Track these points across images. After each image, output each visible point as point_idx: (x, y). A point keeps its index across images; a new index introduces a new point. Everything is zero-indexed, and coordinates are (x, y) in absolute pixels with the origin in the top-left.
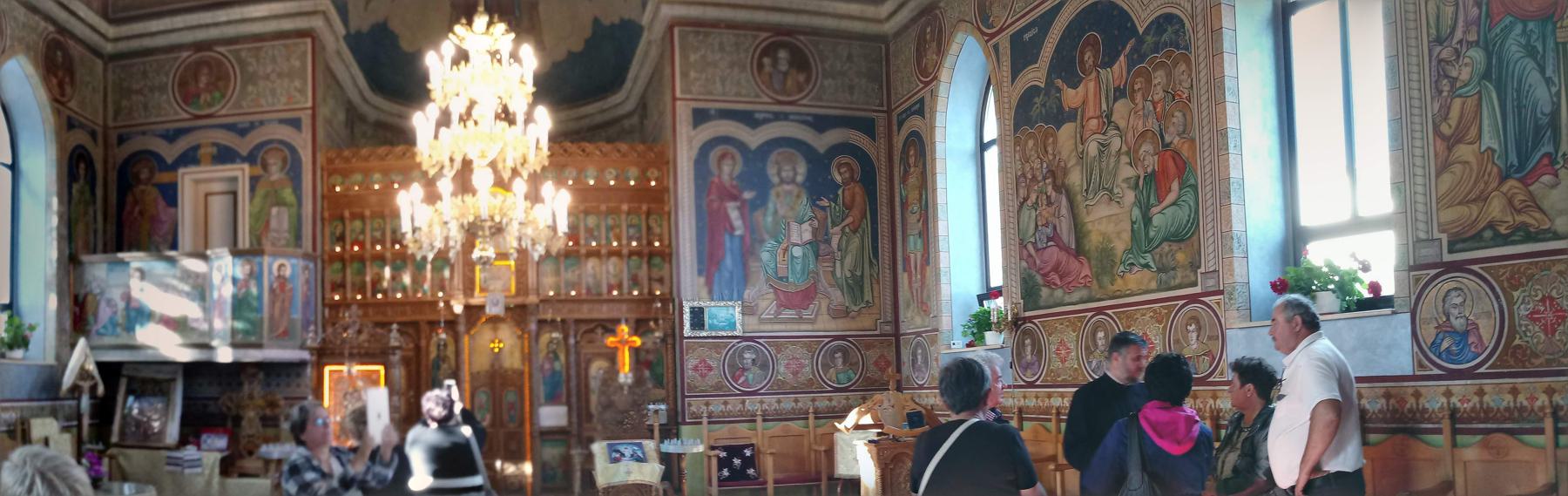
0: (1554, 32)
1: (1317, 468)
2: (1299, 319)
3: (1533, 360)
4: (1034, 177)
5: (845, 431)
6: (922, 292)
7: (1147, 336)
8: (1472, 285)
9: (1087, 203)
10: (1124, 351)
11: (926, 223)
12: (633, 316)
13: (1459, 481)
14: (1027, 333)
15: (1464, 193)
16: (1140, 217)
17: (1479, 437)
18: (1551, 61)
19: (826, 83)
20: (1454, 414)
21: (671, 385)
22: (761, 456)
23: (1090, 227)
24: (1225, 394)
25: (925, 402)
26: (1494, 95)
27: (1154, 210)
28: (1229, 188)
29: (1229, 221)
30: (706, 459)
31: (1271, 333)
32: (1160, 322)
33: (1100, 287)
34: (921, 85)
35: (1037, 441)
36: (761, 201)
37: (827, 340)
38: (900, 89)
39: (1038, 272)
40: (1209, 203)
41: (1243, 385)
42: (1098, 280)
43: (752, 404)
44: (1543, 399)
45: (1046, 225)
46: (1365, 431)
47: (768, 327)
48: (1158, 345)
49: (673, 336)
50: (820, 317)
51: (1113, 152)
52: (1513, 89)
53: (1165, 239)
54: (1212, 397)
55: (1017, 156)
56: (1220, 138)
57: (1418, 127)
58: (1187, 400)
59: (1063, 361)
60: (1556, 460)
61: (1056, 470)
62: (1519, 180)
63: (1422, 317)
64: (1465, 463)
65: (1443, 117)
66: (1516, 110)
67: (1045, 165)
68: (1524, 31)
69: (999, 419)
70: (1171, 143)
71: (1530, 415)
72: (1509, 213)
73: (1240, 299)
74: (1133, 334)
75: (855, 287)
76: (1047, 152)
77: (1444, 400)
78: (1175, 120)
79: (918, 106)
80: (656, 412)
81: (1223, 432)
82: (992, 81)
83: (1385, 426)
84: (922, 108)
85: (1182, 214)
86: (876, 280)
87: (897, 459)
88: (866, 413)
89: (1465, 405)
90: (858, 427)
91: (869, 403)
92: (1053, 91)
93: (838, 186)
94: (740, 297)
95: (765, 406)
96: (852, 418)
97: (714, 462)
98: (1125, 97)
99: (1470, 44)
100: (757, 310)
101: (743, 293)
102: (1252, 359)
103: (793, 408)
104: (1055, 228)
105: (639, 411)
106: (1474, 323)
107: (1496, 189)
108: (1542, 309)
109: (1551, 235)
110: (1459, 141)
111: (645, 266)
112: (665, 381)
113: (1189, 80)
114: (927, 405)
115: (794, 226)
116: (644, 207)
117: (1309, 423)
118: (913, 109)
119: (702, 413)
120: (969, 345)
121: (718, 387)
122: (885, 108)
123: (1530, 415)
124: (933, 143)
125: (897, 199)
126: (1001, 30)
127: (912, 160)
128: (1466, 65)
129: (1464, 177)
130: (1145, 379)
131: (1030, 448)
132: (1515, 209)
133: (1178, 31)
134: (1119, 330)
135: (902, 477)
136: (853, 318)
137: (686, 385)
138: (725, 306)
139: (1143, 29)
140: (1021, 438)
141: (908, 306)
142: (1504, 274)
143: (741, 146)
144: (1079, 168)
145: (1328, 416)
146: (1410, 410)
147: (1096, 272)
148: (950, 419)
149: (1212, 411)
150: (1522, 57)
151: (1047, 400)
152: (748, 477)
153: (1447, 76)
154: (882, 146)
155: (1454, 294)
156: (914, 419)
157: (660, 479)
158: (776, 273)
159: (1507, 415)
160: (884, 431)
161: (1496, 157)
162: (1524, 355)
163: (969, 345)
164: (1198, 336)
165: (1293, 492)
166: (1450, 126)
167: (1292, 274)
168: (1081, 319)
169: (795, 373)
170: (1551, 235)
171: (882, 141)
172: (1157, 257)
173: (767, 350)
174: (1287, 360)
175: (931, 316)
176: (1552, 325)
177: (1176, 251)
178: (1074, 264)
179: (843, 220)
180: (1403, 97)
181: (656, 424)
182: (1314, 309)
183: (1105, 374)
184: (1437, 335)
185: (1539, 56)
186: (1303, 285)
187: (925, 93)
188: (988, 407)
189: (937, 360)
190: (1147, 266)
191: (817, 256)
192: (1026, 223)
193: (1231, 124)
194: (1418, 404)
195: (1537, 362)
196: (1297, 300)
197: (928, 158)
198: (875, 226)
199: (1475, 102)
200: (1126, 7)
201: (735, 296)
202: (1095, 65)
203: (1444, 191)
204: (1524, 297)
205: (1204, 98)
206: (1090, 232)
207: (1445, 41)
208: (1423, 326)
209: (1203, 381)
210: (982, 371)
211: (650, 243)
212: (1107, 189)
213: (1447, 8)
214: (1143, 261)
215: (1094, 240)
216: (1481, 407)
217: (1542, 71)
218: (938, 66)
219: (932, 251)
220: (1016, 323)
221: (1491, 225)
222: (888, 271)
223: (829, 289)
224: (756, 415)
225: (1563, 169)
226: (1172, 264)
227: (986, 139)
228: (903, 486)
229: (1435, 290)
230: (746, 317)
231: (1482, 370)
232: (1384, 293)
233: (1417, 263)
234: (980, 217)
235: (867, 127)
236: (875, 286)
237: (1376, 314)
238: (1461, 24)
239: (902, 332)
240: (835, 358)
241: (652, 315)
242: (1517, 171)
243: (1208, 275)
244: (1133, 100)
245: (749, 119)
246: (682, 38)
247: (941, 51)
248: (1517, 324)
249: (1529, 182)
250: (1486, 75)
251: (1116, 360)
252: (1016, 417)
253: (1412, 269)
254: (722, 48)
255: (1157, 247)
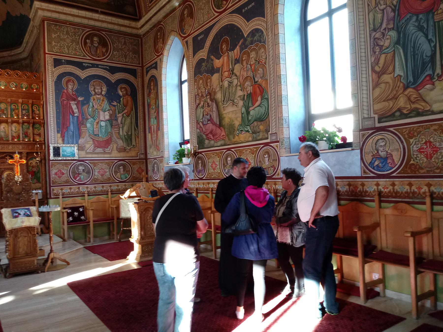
0: (433, 17)
1: (318, 214)
2: (311, 152)
3: (420, 171)
4: (202, 95)
5: (124, 199)
6: (156, 142)
7: (248, 159)
8: (389, 137)
9: (224, 106)
10: (238, 165)
11: (158, 113)
12: (25, 151)
13: (383, 223)
14: (199, 158)
15: (386, 96)
16: (245, 111)
17: (392, 204)
18: (431, 31)
19: (115, 53)
20: (380, 194)
21: (44, 181)
22: (87, 211)
23: (225, 115)
24: (280, 183)
25: (158, 186)
26: (401, 51)
27: (251, 109)
28: (281, 99)
29: (282, 113)
30: (61, 214)
31: (299, 158)
32: (253, 154)
33: (229, 140)
34: (156, 57)
35: (203, 201)
36: (87, 101)
37: (116, 161)
38: (147, 58)
39: (204, 133)
40: (273, 105)
41: (287, 179)
42: (228, 137)
43: (83, 189)
44: (425, 189)
45: (207, 115)
46: (339, 200)
47: (90, 156)
48: (252, 163)
49: (45, 159)
50: (113, 152)
51: (234, 85)
52: (411, 47)
53: (255, 120)
54: (274, 184)
55: (195, 86)
56: (278, 78)
57: (364, 69)
58: (264, 185)
59: (214, 169)
60: (432, 217)
61: (211, 213)
62: (414, 88)
63: (365, 151)
64: (385, 215)
65: (376, 63)
66: (412, 56)
67: (207, 91)
68: (417, 19)
69: (188, 193)
70: (258, 81)
71: (418, 195)
72: (408, 103)
73: (286, 144)
74: (242, 159)
75: (128, 139)
76: (207, 85)
77: (375, 187)
78: (259, 72)
79: (154, 65)
80: (37, 194)
81: (279, 198)
82: (185, 56)
83: (348, 198)
84: (156, 66)
85: (262, 110)
86: (137, 136)
87: (146, 210)
88: (133, 191)
89: (386, 190)
90: (130, 197)
91: (135, 187)
92: (210, 61)
93: (121, 97)
94: (77, 143)
95: (89, 189)
96: (127, 194)
97: (65, 215)
98: (239, 63)
99: (390, 30)
100: (85, 148)
101: (78, 141)
102: (291, 169)
103: (101, 190)
104: (211, 116)
105: (27, 194)
106: (390, 154)
107: (402, 93)
108: (425, 147)
109: (430, 113)
110: (384, 73)
111: (31, 128)
112: (41, 180)
113: (265, 55)
114: (159, 187)
115: (101, 113)
116: (30, 101)
117: (315, 195)
118: (153, 66)
119: (59, 193)
120: (176, 163)
121: (67, 181)
122: (141, 65)
123: (418, 195)
124: (161, 81)
125: (146, 103)
126: (189, 35)
127: (152, 87)
128: (387, 39)
129: (386, 90)
130: (247, 177)
131: (201, 204)
132: (411, 102)
133: (261, 35)
134: (237, 157)
135: (149, 217)
136: (127, 152)
137: (51, 181)
138: (70, 146)
139: (246, 35)
140: (197, 200)
141: (151, 147)
142: (406, 131)
143: (77, 77)
144: (220, 92)
145: (323, 193)
146: (360, 191)
147: (227, 133)
148: (168, 193)
149: (274, 190)
150: (416, 32)
151: (207, 185)
152: (81, 220)
153: (378, 45)
154: (140, 81)
155: (381, 141)
156: (154, 193)
157: (39, 224)
158: (94, 133)
159: (406, 195)
160: (141, 198)
161: (402, 79)
162: (415, 168)
163: (176, 163)
164: (269, 160)
165: (308, 224)
166: (379, 67)
167: (308, 134)
168: (221, 153)
169: (102, 175)
170: (430, 113)
171: (140, 79)
172: (252, 128)
173: (90, 165)
174: (305, 169)
175: (161, 151)
176: (430, 154)
177: (260, 125)
178: (218, 131)
179: (123, 111)
180: (357, 57)
181: (37, 199)
182: (317, 148)
183: (231, 175)
184: (372, 159)
185: (425, 30)
186: (312, 138)
187: (158, 60)
188: (184, 188)
189: (163, 169)
190: (248, 131)
191: (112, 126)
192: (199, 113)
193: (282, 73)
194: (363, 189)
195: (422, 171)
196: (310, 144)
197: (159, 87)
198: (137, 114)
199: (392, 55)
200: (239, 26)
201: (75, 142)
202: (227, 50)
203: (376, 96)
204: (416, 142)
205: (271, 63)
206: (224, 118)
207: (377, 30)
208: (366, 155)
209: (270, 178)
210: (181, 174)
211: (33, 118)
212: (232, 100)
213: (379, 15)
214: (246, 129)
215: (226, 121)
216: (394, 191)
217: (426, 36)
218: (163, 49)
219: (160, 125)
220: (195, 154)
221: (399, 110)
222: (142, 133)
223: (117, 140)
224: (85, 194)
225: (437, 81)
226: (258, 130)
227: (183, 80)
228: (149, 220)
229: (371, 140)
230: (80, 151)
231: (394, 175)
232: (348, 141)
233: (363, 128)
234: (180, 111)
235: (133, 72)
236: (137, 139)
237: (344, 150)
238: (385, 21)
239: (148, 158)
240: (120, 169)
241: (35, 151)
242: (413, 84)
243: (273, 135)
244: (242, 64)
245: (80, 66)
246: (49, 25)
247: (164, 43)
248: (412, 154)
249: (419, 89)
250: (398, 42)
251: (235, 169)
252: (195, 192)
253: (361, 130)
254: (68, 33)
255: (252, 123)
